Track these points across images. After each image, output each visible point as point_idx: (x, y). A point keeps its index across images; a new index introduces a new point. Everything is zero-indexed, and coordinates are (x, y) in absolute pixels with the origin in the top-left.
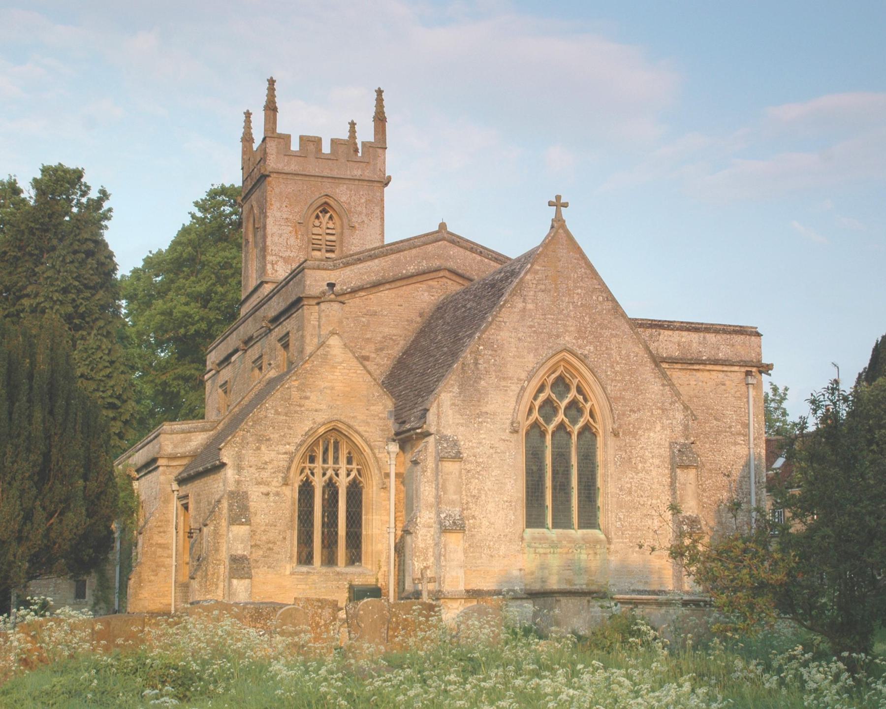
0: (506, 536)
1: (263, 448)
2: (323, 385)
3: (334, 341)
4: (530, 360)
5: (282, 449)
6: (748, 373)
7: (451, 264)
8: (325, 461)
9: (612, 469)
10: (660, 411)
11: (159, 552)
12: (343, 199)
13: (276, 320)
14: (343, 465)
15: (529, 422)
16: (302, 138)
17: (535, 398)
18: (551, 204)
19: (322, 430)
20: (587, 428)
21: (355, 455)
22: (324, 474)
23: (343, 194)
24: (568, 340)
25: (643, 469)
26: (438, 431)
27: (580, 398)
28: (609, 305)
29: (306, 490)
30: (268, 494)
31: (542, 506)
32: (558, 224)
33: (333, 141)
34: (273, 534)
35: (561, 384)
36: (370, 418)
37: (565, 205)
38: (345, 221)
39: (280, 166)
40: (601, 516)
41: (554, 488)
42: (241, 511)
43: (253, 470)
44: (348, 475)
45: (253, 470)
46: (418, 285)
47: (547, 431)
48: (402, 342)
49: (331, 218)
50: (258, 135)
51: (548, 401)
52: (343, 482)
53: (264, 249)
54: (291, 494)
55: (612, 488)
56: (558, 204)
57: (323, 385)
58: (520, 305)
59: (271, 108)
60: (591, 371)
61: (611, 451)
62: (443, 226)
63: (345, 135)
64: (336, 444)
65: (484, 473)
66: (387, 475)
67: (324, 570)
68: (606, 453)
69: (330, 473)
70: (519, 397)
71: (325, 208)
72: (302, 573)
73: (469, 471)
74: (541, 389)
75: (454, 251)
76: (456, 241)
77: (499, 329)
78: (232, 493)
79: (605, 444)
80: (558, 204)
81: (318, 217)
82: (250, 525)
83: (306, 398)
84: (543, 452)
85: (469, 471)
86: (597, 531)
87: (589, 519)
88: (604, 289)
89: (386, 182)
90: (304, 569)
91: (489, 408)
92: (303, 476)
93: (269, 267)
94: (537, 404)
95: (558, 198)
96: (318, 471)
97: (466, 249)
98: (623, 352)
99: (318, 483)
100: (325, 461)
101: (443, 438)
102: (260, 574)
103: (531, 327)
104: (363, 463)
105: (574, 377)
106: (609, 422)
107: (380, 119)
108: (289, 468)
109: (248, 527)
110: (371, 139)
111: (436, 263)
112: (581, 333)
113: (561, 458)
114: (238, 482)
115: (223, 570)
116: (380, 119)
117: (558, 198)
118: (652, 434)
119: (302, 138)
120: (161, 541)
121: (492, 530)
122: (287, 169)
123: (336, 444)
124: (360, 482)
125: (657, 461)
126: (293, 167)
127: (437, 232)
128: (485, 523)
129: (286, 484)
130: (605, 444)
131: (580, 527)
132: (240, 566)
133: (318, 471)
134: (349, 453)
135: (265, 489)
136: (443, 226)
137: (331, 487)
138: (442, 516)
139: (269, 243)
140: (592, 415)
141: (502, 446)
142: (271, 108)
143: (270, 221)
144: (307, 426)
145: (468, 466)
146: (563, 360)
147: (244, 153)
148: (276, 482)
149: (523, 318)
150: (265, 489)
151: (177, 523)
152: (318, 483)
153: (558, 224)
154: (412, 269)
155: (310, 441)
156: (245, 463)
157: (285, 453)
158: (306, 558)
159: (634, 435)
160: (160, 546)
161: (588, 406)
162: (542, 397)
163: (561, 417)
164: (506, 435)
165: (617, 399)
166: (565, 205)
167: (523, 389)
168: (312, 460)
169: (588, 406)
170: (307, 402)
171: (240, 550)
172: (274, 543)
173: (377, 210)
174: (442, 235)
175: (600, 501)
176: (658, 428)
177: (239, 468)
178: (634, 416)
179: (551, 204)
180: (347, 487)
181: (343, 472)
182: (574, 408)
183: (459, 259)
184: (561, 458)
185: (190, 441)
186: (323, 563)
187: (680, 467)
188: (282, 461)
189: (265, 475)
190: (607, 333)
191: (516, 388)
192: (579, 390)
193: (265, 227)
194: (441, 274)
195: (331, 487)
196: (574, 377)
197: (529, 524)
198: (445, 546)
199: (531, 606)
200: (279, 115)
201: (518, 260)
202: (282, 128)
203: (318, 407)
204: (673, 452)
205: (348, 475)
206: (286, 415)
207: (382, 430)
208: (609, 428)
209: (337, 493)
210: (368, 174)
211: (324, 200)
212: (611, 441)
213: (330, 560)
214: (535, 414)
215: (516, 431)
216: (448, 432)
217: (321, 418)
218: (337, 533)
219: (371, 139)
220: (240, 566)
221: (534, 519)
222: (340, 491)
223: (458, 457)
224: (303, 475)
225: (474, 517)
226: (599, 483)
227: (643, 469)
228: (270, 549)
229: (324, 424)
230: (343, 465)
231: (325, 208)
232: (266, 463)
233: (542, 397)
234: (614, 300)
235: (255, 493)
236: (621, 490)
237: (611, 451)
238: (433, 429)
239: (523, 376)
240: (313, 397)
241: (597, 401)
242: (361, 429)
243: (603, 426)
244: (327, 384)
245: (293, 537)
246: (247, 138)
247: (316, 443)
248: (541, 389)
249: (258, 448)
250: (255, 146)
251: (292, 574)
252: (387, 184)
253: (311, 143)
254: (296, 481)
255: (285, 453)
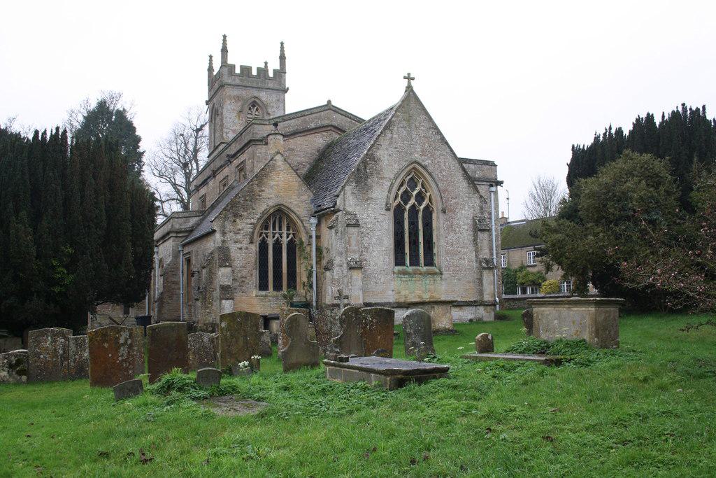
0: (384, 271)
1: (238, 220)
2: (272, 183)
3: (278, 157)
4: (396, 167)
5: (249, 221)
6: (492, 186)
7: (333, 123)
8: (274, 229)
9: (442, 231)
10: (467, 199)
11: (173, 286)
12: (264, 99)
13: (234, 156)
14: (284, 231)
15: (395, 204)
16: (241, 66)
17: (399, 189)
18: (405, 78)
19: (272, 211)
20: (427, 207)
21: (291, 225)
22: (274, 237)
23: (264, 96)
24: (417, 156)
25: (459, 231)
26: (344, 209)
27: (423, 190)
28: (438, 137)
29: (263, 247)
30: (241, 249)
31: (403, 253)
32: (409, 89)
33: (258, 69)
34: (244, 273)
35: (413, 183)
36: (299, 202)
37: (413, 79)
38: (265, 110)
39: (230, 81)
40: (435, 258)
41: (410, 243)
42: (224, 257)
43: (232, 234)
44: (288, 237)
45: (232, 234)
46: (316, 134)
47: (405, 209)
48: (308, 166)
49: (257, 110)
50: (217, 66)
51: (406, 192)
52: (285, 241)
53: (222, 125)
54: (254, 248)
55: (442, 242)
56: (409, 78)
57: (272, 183)
58: (390, 135)
59: (224, 51)
60: (430, 174)
61: (441, 221)
62: (329, 102)
63: (262, 66)
64: (280, 218)
65: (371, 234)
66: (311, 237)
67: (275, 293)
68: (438, 222)
69: (277, 236)
70: (390, 191)
71: (254, 104)
72: (262, 296)
73: (362, 233)
74: (402, 185)
75: (335, 116)
76: (337, 111)
77: (378, 149)
78: (219, 248)
79: (438, 217)
80: (409, 78)
81: (250, 109)
82: (231, 267)
83: (263, 191)
84: (403, 222)
85: (362, 233)
86: (434, 268)
87: (429, 261)
88: (436, 128)
89: (286, 91)
90: (263, 293)
91: (374, 195)
92: (261, 238)
93: (224, 135)
94: (400, 193)
95: (409, 74)
96: (270, 235)
97: (342, 115)
98: (447, 164)
99: (270, 241)
100: (274, 229)
101: (347, 213)
102: (238, 296)
103: (396, 148)
104: (296, 230)
105: (419, 177)
106: (440, 204)
107: (282, 58)
108: (253, 233)
109: (230, 268)
110: (278, 67)
111: (326, 122)
112: (423, 152)
113: (413, 224)
114: (224, 242)
115: (217, 293)
116: (282, 58)
117: (409, 74)
118: (463, 212)
119: (241, 66)
120: (173, 280)
121: (376, 268)
122: (234, 83)
123: (280, 218)
124: (295, 241)
125: (466, 227)
126: (237, 81)
127: (326, 105)
128: (372, 263)
129: (251, 242)
130: (438, 217)
131: (425, 265)
132: (227, 292)
133: (270, 235)
134: (288, 224)
135: (239, 245)
136: (329, 102)
137: (277, 245)
138: (349, 259)
139: (224, 122)
140: (430, 200)
141: (381, 218)
142: (224, 51)
143: (225, 111)
144: (263, 208)
145: (362, 230)
146: (414, 168)
147: (209, 77)
148: (246, 241)
149: (391, 143)
150: (239, 245)
151: (183, 269)
152: (270, 241)
153: (409, 89)
154: (312, 125)
155: (266, 216)
156: (227, 230)
157: (251, 224)
158: (263, 286)
159: (454, 212)
160: (173, 283)
161: (428, 194)
162: (403, 189)
163: (412, 201)
164: (383, 212)
165: (444, 191)
166: (413, 79)
167: (392, 184)
168: (267, 228)
169: (428, 194)
170: (263, 194)
171: (227, 282)
172: (246, 278)
173: (281, 105)
174: (329, 107)
175: (435, 251)
176: (467, 208)
177: (224, 233)
178: (453, 201)
179: (405, 78)
180: (287, 245)
181: (284, 235)
182: (420, 197)
183: (338, 120)
184: (413, 224)
185: (189, 222)
186: (274, 289)
187: (480, 230)
188: (249, 229)
189: (239, 237)
190: (438, 153)
191: (388, 184)
192: (423, 186)
193: (222, 114)
194: (329, 129)
195: (277, 245)
196: (420, 178)
197: (397, 264)
198: (351, 277)
199: (594, 309)
200: (228, 54)
201: (377, 120)
202: (230, 61)
203: (270, 196)
204: (476, 222)
205: (288, 237)
206: (251, 201)
207: (308, 210)
208: (440, 207)
209: (282, 248)
210: (276, 86)
211: (253, 99)
212: (441, 215)
213: (278, 287)
214: (399, 200)
215: (388, 209)
216: (349, 209)
217: (271, 203)
218: (282, 272)
219: (278, 67)
220: (227, 292)
221: (399, 261)
222: (283, 246)
223: (357, 225)
224: (261, 238)
225: (366, 260)
226: (435, 240)
227: (459, 231)
228: (243, 281)
229: (274, 207)
230: (284, 231)
231: (254, 104)
232: (239, 230)
233: (403, 189)
234: (441, 134)
235: (233, 248)
236: (447, 243)
237: (441, 221)
238: (341, 208)
239: (392, 176)
240: (266, 190)
241: (433, 192)
242: (295, 210)
243: (437, 207)
244: (274, 183)
245: (256, 273)
246: (210, 69)
247: (269, 218)
248: (402, 185)
249: (234, 221)
250: (215, 73)
251: (257, 296)
252: (286, 92)
253: (246, 70)
254: (257, 240)
255: (251, 224)
